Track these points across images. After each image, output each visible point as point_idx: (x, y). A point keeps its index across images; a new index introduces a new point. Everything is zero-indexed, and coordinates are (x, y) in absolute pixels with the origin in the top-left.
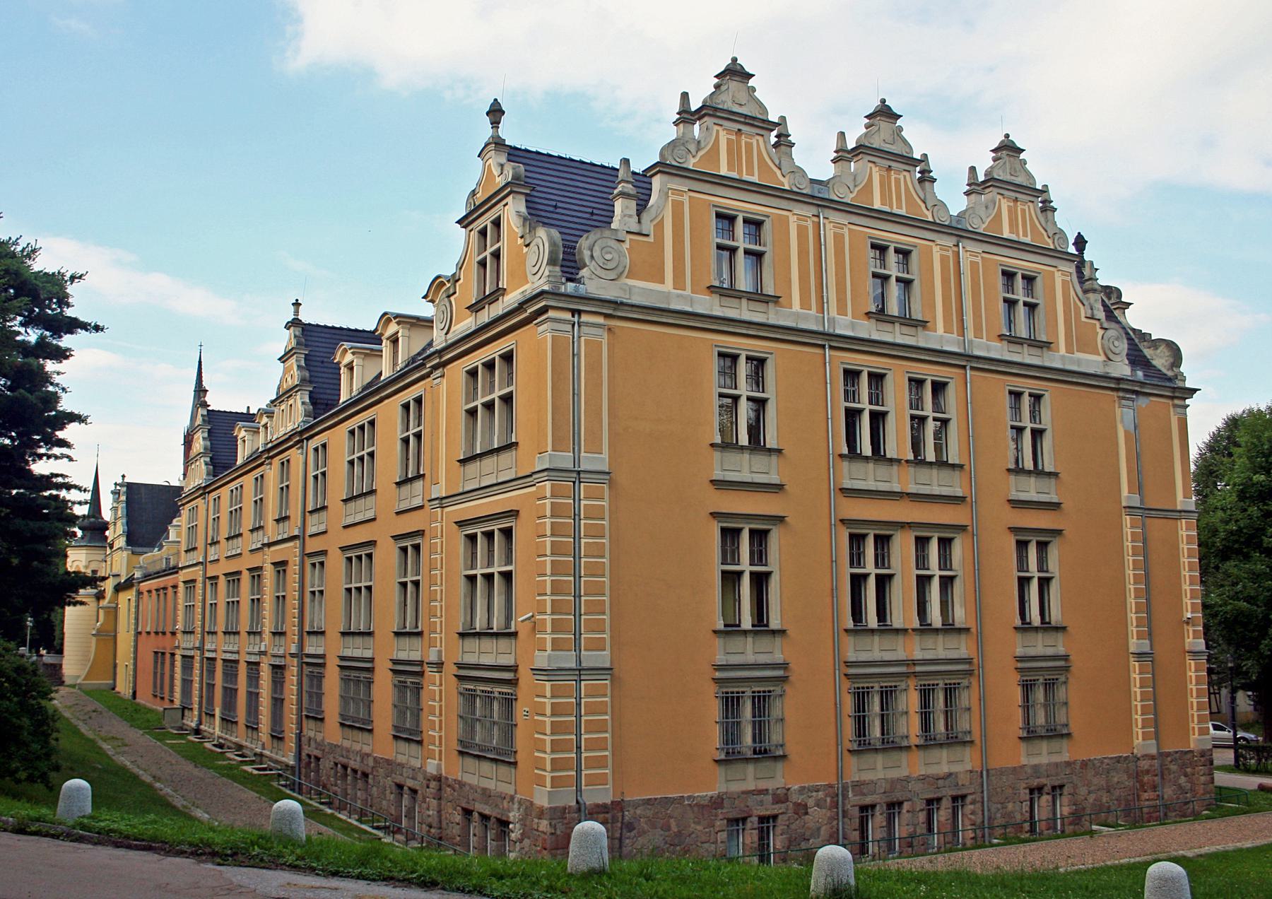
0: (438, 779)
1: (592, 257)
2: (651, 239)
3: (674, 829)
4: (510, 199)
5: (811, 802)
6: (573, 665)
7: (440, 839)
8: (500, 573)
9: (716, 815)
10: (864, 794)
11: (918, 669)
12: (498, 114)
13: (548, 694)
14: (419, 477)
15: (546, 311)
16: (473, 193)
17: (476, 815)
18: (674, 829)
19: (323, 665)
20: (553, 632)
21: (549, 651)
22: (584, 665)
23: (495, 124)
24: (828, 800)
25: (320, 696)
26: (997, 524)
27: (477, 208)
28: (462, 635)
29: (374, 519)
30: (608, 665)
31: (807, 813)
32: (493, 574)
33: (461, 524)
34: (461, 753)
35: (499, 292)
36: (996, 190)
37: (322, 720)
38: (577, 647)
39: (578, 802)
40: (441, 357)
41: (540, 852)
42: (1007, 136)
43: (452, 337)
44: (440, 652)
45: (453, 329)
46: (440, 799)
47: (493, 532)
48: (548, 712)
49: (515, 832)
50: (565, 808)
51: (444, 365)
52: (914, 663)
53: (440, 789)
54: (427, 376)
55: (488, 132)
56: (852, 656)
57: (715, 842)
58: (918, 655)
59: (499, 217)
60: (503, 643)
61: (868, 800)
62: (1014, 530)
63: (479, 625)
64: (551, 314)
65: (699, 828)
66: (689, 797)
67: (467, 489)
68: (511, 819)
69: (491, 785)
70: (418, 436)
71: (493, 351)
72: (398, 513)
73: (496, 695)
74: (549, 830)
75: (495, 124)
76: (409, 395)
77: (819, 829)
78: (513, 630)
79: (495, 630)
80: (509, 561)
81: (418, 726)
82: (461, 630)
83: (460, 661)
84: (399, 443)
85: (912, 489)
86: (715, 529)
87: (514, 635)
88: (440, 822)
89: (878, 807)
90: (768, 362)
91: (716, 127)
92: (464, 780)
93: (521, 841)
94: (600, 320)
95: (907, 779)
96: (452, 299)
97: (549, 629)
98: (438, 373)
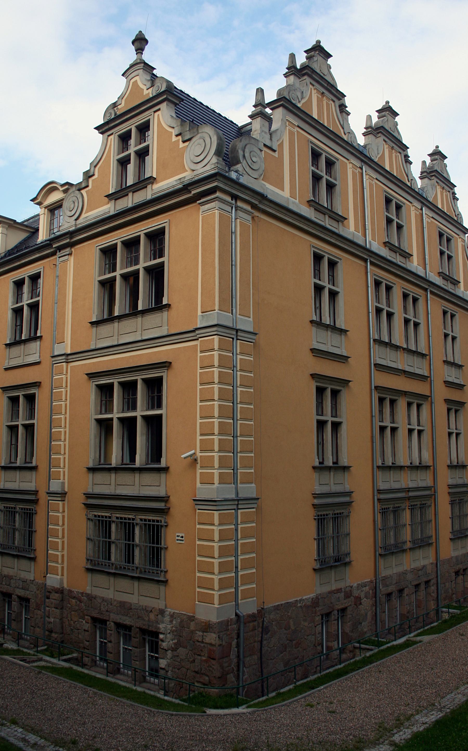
0: (60, 591)
1: (244, 156)
2: (276, 155)
3: (293, 628)
4: (163, 106)
5: (362, 595)
6: (233, 496)
7: (62, 642)
8: (143, 417)
9: (316, 613)
10: (387, 586)
11: (411, 494)
12: (144, 43)
13: (216, 522)
14: (34, 338)
15: (215, 192)
16: (114, 105)
17: (111, 625)
18: (293, 628)
19: (36, 502)
20: (220, 467)
21: (216, 485)
22: (240, 495)
23: (140, 50)
24: (371, 591)
25: (31, 533)
26: (440, 393)
27: (117, 117)
28: (92, 470)
29: (38, 363)
30: (254, 496)
31: (361, 604)
32: (17, 426)
33: (91, 376)
34: (88, 570)
35: (143, 183)
36: (436, 179)
37: (165, 582)
38: (235, 482)
39: (236, 614)
40: (71, 238)
41: (206, 661)
42: (437, 147)
43: (82, 222)
44: (63, 483)
45: (83, 216)
46: (62, 608)
47: (111, 386)
48: (216, 537)
49: (167, 641)
50: (228, 621)
51: (72, 245)
52: (408, 490)
53: (62, 600)
54: (54, 254)
55: (132, 57)
56: (383, 486)
57: (315, 635)
58: (412, 485)
59: (148, 121)
60: (27, 474)
61: (390, 589)
62: (447, 401)
63: (389, 462)
64: (218, 194)
65: (306, 624)
66: (301, 600)
67: (121, 342)
68: (162, 630)
69: (133, 599)
70: (34, 307)
71: (140, 230)
72: (6, 369)
73: (114, 519)
74: (218, 642)
75: (140, 50)
76: (25, 273)
77: (366, 615)
78: (34, 464)
79: (114, 465)
80: (31, 415)
81: (30, 544)
82: (91, 465)
83: (90, 491)
84: (9, 314)
85: (407, 369)
86: (313, 385)
87: (35, 468)
88: (62, 627)
89: (394, 594)
90: (339, 265)
91: (311, 86)
92: (94, 593)
93: (174, 650)
94: (248, 208)
95: (405, 573)
96: (83, 192)
97: (216, 465)
98: (67, 251)
